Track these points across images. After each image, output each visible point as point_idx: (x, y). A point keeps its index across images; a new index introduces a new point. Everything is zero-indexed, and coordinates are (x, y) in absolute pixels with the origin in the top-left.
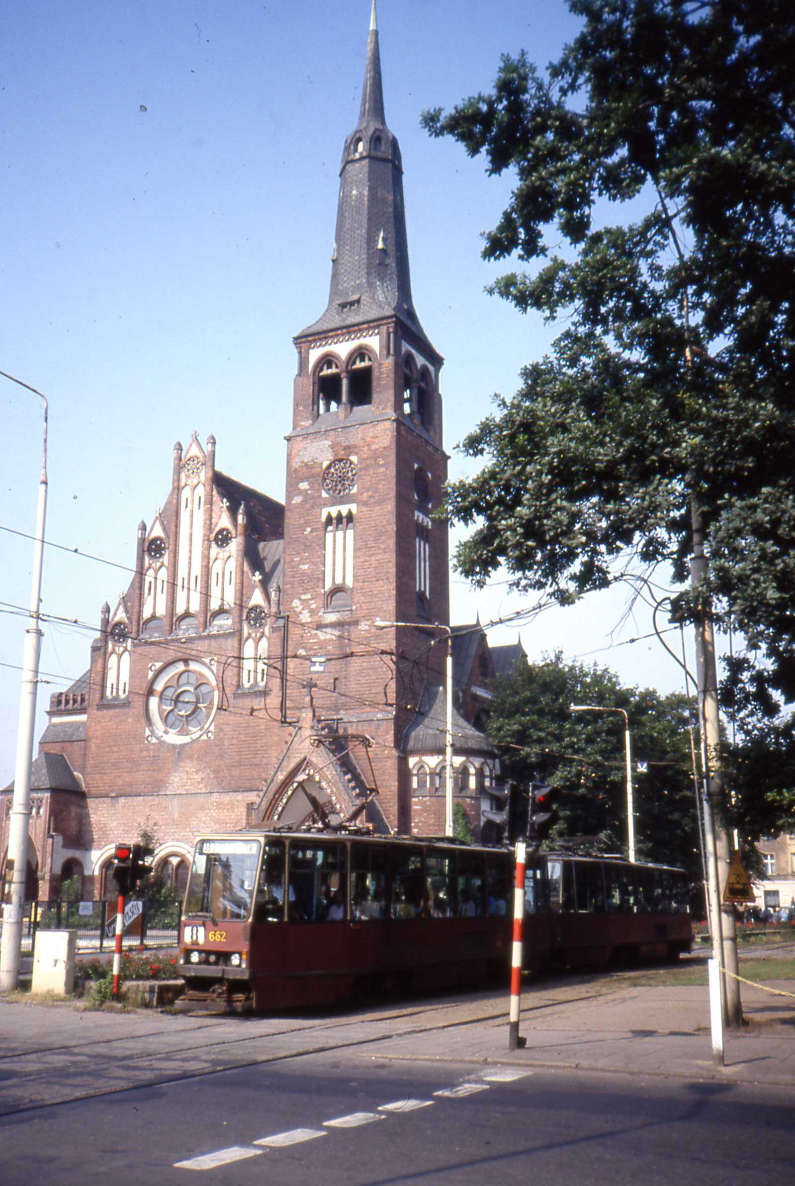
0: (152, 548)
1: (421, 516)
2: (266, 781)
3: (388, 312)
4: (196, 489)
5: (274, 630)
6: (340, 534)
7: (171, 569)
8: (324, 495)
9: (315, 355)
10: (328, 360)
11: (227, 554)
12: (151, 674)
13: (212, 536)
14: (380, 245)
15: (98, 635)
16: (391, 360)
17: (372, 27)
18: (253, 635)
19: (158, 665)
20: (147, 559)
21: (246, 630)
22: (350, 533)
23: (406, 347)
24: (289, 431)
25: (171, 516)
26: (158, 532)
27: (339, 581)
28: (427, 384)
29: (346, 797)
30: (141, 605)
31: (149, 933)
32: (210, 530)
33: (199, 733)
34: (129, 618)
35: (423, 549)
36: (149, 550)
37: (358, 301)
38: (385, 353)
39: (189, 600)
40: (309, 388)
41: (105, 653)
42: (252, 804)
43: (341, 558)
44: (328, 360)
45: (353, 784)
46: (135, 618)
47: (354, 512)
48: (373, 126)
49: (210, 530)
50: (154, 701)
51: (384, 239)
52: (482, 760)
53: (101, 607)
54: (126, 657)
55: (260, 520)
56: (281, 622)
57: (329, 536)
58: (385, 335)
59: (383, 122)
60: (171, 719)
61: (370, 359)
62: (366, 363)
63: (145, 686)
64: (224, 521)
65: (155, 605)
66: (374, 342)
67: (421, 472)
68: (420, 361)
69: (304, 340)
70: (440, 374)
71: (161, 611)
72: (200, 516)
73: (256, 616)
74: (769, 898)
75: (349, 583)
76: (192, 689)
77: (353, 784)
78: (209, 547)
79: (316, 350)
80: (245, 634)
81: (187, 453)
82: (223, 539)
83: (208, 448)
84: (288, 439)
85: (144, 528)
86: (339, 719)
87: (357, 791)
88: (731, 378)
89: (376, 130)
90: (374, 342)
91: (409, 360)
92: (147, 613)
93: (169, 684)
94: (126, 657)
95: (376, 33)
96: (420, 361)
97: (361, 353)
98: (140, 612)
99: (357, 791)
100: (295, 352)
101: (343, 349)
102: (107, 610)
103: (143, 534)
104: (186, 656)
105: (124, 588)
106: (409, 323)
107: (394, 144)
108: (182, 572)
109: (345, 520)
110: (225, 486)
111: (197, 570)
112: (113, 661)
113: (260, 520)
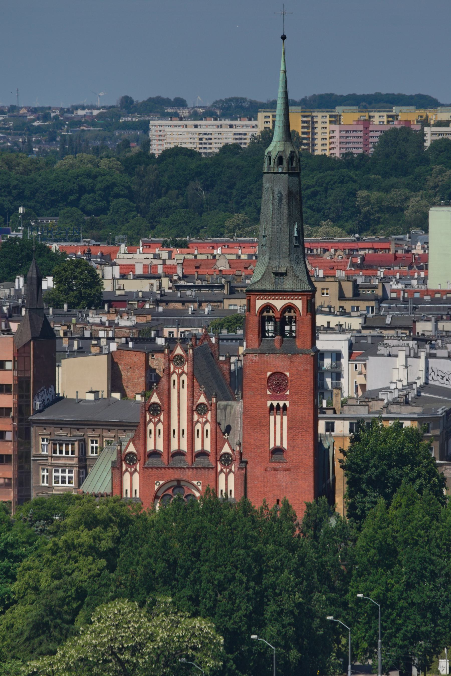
7: (166, 424)
8: (269, 393)
9: (260, 303)
10: (268, 307)
11: (204, 420)
12: (156, 487)
13: (194, 408)
17: (282, 68)
19: (161, 482)
22: (285, 418)
27: (278, 444)
31: (61, 395)
32: (193, 404)
37: (286, 274)
38: (305, 310)
39: (180, 443)
41: (121, 471)
44: (268, 307)
46: (142, 452)
47: (288, 405)
49: (193, 404)
54: (136, 476)
57: (272, 418)
61: (295, 312)
70: (265, 101)
72: (184, 392)
73: (226, 460)
74: (430, 360)
75: (285, 446)
78: (193, 415)
79: (260, 301)
80: (219, 469)
90: (298, 303)
93: (166, 493)
95: (285, 71)
97: (289, 308)
98: (145, 448)
101: (279, 304)
108: (174, 426)
112: (127, 476)
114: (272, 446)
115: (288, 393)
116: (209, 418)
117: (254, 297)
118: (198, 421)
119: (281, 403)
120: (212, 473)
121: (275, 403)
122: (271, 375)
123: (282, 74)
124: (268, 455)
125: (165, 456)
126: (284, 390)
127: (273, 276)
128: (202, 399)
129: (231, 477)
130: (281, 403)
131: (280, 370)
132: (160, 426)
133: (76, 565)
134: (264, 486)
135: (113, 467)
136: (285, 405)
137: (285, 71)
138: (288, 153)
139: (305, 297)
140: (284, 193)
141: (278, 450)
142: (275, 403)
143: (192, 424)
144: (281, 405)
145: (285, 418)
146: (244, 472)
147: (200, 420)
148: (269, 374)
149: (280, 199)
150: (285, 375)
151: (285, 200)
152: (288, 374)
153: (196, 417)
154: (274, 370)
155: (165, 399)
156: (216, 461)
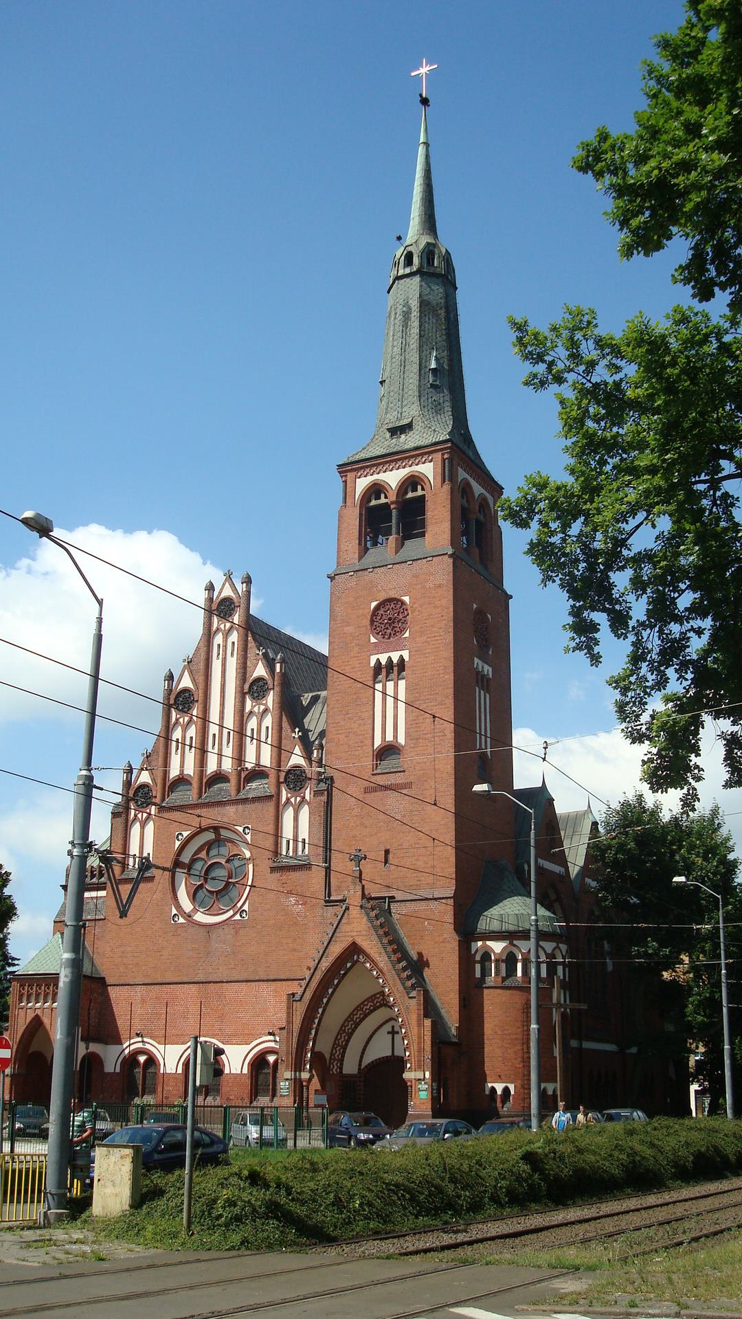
0: (179, 701)
1: (480, 663)
2: (309, 968)
3: (444, 436)
4: (229, 640)
5: (317, 793)
6: (390, 685)
8: (373, 640)
9: (362, 483)
10: (376, 490)
11: (262, 707)
13: (247, 687)
14: (433, 366)
15: (119, 799)
16: (447, 487)
17: (422, 140)
18: (293, 800)
20: (215, 619)
21: (284, 795)
22: (402, 683)
23: (462, 474)
24: (332, 568)
25: (201, 663)
26: (187, 682)
27: (390, 737)
28: (485, 516)
29: (401, 988)
30: (166, 763)
33: (231, 913)
34: (153, 780)
35: (483, 700)
36: (176, 705)
38: (439, 478)
39: (221, 760)
40: (353, 518)
41: (127, 820)
42: (293, 995)
43: (390, 715)
44: (376, 490)
45: (408, 972)
46: (159, 781)
47: (406, 658)
48: (426, 239)
50: (181, 877)
51: (437, 359)
52: (555, 944)
53: (165, 672)
55: (295, 678)
56: (323, 786)
58: (440, 463)
59: (436, 237)
60: (201, 894)
62: (420, 492)
63: (172, 856)
64: (260, 671)
65: (182, 763)
66: (427, 469)
67: (480, 613)
68: (478, 489)
69: (348, 469)
71: (190, 770)
72: (233, 663)
73: (296, 779)
75: (401, 740)
76: (223, 861)
77: (408, 972)
79: (363, 479)
81: (220, 593)
82: (256, 689)
83: (241, 588)
84: (332, 578)
85: (170, 677)
86: (390, 898)
87: (413, 981)
88: (677, 858)
89: (428, 244)
90: (427, 469)
91: (465, 490)
92: (174, 772)
94: (150, 827)
96: (478, 489)
97: (413, 482)
98: (166, 773)
99: (413, 981)
100: (339, 480)
101: (393, 478)
102: (170, 677)
103: (170, 686)
104: (216, 824)
105: (149, 743)
106: (465, 448)
107: (447, 258)
109: (395, 669)
110: (259, 633)
111: (229, 722)
112: (135, 830)
113: (295, 678)
114: (378, 742)
115: (407, 635)
116: (270, 705)
117: (354, 474)
118: (251, 712)
119: (395, 657)
120: (270, 807)
121: (383, 659)
122: (377, 608)
123: (421, 150)
124: (368, 762)
125: (195, 784)
126: (402, 630)
127: (388, 435)
128: (260, 671)
129: (305, 812)
130: (395, 657)
131: (393, 594)
132: (192, 732)
133: (632, 1297)
134: (362, 824)
135: (115, 815)
136: (402, 659)
137: (426, 144)
138: (422, 245)
139: (438, 456)
140: (415, 304)
141: (388, 751)
142: (383, 659)
143: (242, 718)
144: (395, 661)
145: (402, 683)
146: (324, 798)
147: (256, 709)
148: (374, 604)
149: (407, 315)
150: (403, 603)
151: (415, 314)
152: (406, 599)
153: (249, 703)
154: (383, 596)
155: (201, 679)
156: (279, 784)
